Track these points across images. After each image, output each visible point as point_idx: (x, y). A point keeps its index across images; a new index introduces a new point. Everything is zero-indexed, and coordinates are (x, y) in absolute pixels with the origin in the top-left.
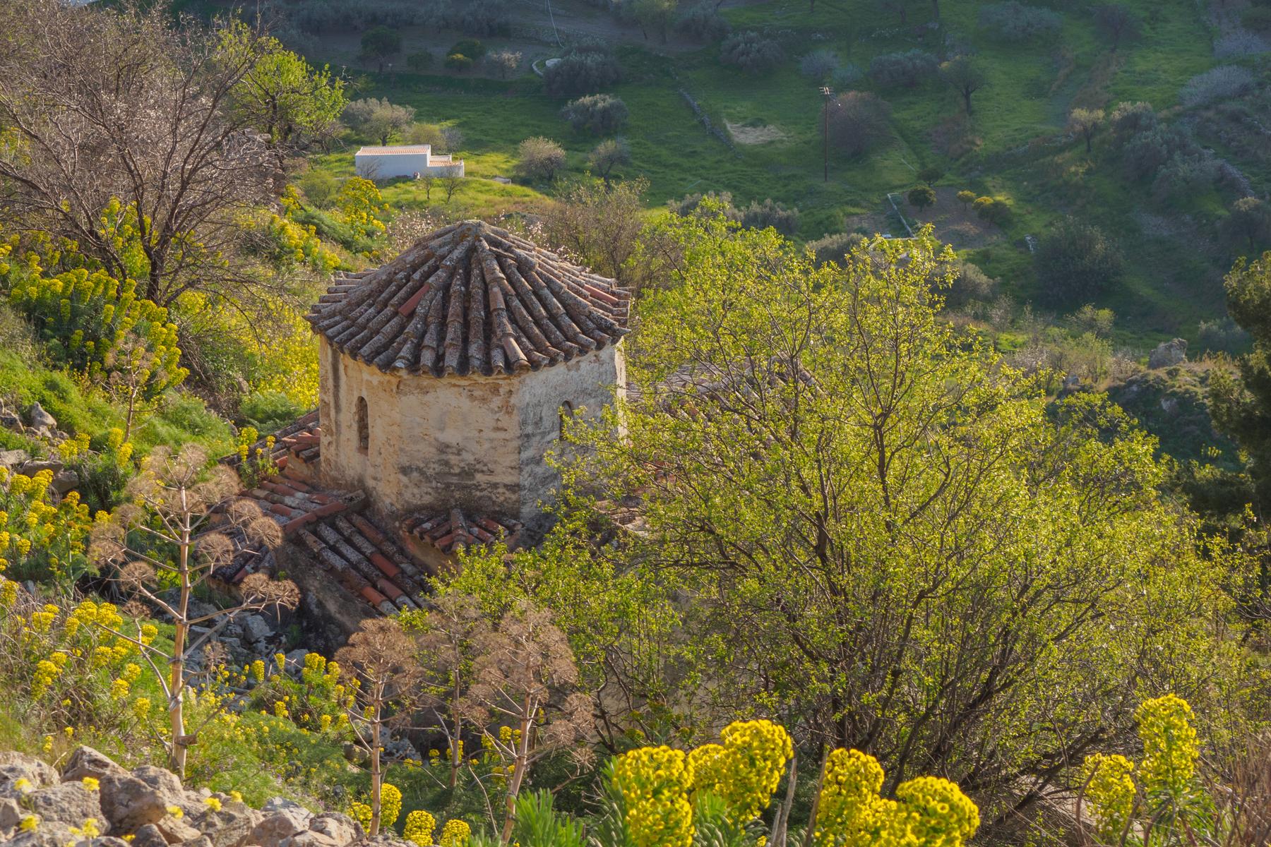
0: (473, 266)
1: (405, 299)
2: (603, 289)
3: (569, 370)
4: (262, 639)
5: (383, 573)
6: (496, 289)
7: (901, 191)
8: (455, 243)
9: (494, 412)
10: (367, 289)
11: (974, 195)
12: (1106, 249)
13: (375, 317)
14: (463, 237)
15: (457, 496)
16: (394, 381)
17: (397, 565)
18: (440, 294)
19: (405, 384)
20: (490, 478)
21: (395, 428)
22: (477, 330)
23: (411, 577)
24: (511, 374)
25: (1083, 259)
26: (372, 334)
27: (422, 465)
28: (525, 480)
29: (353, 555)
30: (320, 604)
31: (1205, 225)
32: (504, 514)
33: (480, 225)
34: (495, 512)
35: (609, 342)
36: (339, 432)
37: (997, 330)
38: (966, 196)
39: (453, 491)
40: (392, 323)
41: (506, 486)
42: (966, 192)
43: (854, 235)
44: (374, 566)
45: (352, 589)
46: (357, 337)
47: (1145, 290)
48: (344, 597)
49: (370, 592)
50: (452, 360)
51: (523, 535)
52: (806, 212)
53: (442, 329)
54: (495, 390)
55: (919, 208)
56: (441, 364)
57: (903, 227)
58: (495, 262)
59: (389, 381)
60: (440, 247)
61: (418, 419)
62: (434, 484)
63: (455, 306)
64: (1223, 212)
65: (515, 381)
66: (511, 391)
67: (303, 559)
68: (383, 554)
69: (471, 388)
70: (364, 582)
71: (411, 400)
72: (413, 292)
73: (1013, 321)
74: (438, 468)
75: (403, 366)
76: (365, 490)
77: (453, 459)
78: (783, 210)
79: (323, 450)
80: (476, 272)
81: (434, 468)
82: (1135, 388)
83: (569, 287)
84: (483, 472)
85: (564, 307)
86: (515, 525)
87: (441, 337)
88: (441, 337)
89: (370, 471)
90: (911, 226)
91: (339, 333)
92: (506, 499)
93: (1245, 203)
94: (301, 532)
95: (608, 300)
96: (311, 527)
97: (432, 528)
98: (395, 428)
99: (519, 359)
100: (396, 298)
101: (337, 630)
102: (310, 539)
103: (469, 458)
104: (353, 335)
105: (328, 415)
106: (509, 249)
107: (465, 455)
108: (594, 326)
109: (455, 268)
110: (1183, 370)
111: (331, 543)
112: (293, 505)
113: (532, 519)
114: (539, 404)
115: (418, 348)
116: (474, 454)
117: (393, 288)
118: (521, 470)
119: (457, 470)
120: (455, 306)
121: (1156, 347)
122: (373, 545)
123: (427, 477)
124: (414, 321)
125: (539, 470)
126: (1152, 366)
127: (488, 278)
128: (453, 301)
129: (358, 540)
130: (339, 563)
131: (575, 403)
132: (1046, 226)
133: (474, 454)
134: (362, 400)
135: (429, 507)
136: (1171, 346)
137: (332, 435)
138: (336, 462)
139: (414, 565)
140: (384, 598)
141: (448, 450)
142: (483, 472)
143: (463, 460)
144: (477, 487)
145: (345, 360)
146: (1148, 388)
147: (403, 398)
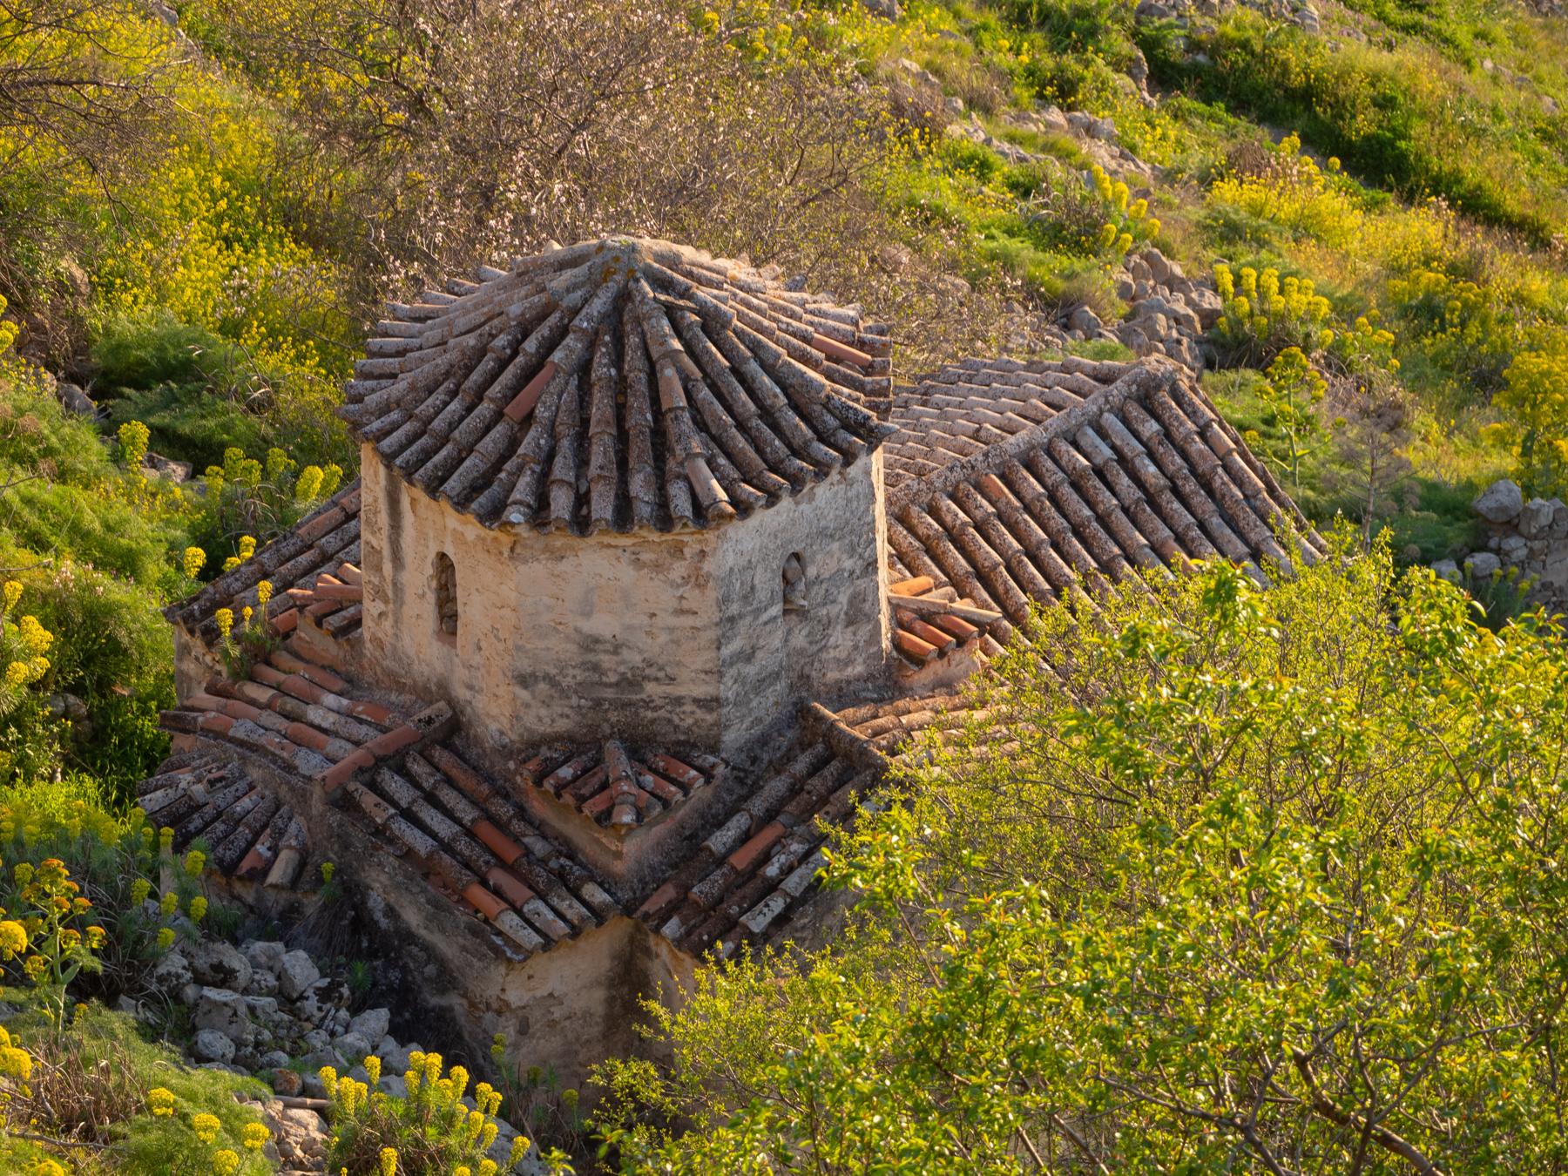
0: (628, 328)
4: (310, 993)
5: (494, 854)
6: (670, 372)
13: (462, 419)
14: (607, 274)
16: (505, 539)
17: (517, 840)
18: (574, 381)
19: (524, 547)
20: (669, 689)
21: (506, 612)
22: (640, 447)
23: (543, 862)
24: (704, 527)
26: (460, 451)
27: (553, 671)
28: (728, 689)
29: (444, 828)
30: (391, 912)
32: (694, 746)
34: (679, 743)
41: (696, 701)
45: (445, 887)
48: (436, 905)
49: (478, 894)
50: (602, 506)
53: (581, 445)
54: (678, 551)
56: (584, 511)
59: (495, 539)
60: (568, 291)
62: (574, 701)
63: (601, 406)
65: (710, 535)
66: (703, 552)
67: (359, 837)
68: (491, 818)
69: (637, 549)
70: (466, 876)
71: (536, 570)
72: (529, 374)
74: (581, 675)
75: (521, 518)
76: (451, 702)
77: (607, 661)
79: (367, 622)
80: (633, 340)
81: (577, 675)
84: (657, 679)
85: (784, 389)
86: (713, 766)
87: (582, 462)
88: (582, 462)
89: (461, 674)
91: (402, 448)
92: (697, 721)
94: (351, 786)
96: (367, 776)
97: (576, 778)
98: (506, 612)
99: (716, 501)
102: (368, 800)
103: (636, 659)
104: (427, 454)
107: (626, 654)
109: (596, 333)
111: (404, 804)
112: (325, 725)
113: (740, 750)
115: (543, 483)
116: (640, 652)
117: (488, 363)
118: (721, 674)
119: (613, 678)
120: (601, 406)
122: (474, 803)
123: (563, 691)
124: (532, 433)
125: (750, 670)
127: (655, 352)
128: (595, 390)
129: (448, 796)
131: (807, 554)
133: (640, 652)
134: (442, 556)
135: (569, 738)
137: (386, 602)
138: (395, 648)
139: (544, 837)
140: (504, 905)
141: (600, 647)
142: (657, 679)
143: (623, 662)
144: (647, 704)
145: (409, 495)
147: (522, 568)
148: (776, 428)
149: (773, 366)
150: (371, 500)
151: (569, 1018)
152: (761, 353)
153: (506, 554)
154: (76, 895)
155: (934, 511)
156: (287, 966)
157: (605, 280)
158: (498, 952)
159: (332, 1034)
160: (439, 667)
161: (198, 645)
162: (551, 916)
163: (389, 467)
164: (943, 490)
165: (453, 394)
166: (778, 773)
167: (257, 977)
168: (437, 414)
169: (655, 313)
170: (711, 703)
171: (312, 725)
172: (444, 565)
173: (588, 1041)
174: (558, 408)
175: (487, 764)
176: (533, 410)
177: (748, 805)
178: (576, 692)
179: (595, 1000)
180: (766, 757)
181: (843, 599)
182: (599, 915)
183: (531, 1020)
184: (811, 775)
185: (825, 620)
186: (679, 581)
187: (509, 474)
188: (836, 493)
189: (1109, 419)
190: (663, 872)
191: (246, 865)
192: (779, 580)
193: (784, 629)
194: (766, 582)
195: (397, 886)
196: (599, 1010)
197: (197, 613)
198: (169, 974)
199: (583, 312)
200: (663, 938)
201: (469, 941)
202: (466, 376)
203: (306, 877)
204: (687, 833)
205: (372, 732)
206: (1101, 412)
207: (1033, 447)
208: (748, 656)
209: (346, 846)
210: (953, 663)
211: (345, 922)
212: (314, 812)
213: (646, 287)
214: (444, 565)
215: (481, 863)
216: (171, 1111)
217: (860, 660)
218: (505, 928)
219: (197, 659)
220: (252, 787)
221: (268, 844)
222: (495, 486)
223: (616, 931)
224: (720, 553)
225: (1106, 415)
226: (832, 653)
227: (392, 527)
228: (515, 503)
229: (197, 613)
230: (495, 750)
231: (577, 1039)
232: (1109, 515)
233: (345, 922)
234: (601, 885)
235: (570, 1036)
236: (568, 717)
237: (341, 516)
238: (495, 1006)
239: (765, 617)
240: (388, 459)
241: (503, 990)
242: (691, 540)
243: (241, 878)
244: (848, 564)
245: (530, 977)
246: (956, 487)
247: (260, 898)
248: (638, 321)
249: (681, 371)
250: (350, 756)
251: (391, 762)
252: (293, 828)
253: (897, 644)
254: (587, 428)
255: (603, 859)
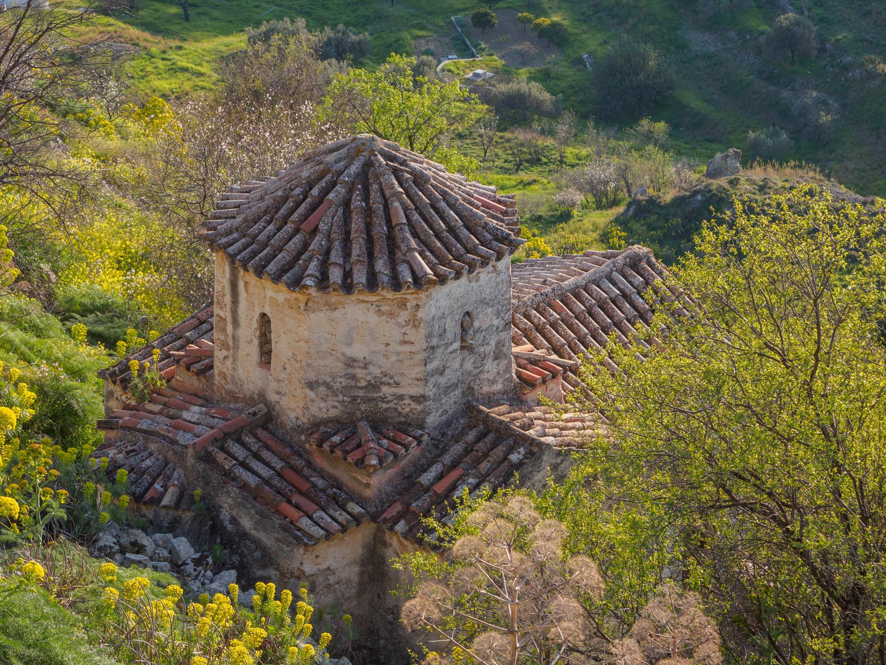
0: (371, 181)
1: (306, 216)
2: (489, 198)
3: (470, 282)
4: (189, 561)
5: (295, 487)
6: (396, 204)
7: (463, 14)
8: (351, 159)
9: (400, 326)
10: (263, 205)
11: (532, 16)
12: (658, 65)
13: (275, 234)
14: (358, 152)
15: (363, 409)
16: (302, 298)
17: (307, 479)
18: (341, 210)
19: (314, 302)
20: (395, 390)
21: (302, 344)
22: (380, 245)
23: (323, 491)
24: (420, 289)
25: (637, 75)
26: (275, 251)
27: (328, 379)
28: (430, 391)
29: (265, 472)
30: (234, 521)
31: (749, 40)
32: (410, 425)
33: (373, 139)
34: (400, 423)
35: (507, 253)
36: (236, 347)
37: (562, 143)
38: (525, 17)
39: (359, 404)
40: (295, 240)
41: (411, 397)
42: (525, 14)
43: (425, 57)
44: (285, 479)
45: (267, 504)
46: (261, 255)
47: (695, 103)
48: (261, 514)
49: (286, 508)
50: (360, 276)
51: (427, 445)
52: (376, 35)
53: (345, 245)
54: (403, 304)
55: (481, 29)
56: (349, 281)
57: (467, 48)
58: (393, 177)
59: (296, 299)
60: (336, 162)
61: (325, 335)
62: (340, 398)
63: (357, 223)
64: (764, 27)
65: (422, 295)
66: (418, 305)
67: (215, 477)
70: (279, 498)
71: (319, 317)
72: (313, 208)
73: (576, 135)
75: (313, 284)
76: (267, 404)
77: (360, 373)
78: (355, 34)
79: (217, 364)
80: (375, 187)
81: (341, 382)
82: (699, 197)
83: (464, 199)
84: (389, 384)
85: (461, 218)
86: (422, 435)
87: (347, 254)
88: (347, 254)
89: (273, 385)
90: (475, 47)
91: (240, 252)
93: (786, 19)
94: (210, 449)
95: (497, 209)
96: (219, 443)
97: (342, 442)
99: (426, 274)
100: (295, 215)
101: (253, 546)
102: (220, 456)
103: (377, 372)
104: (255, 254)
105: (224, 330)
106: (404, 163)
107: (371, 369)
108: (491, 237)
109: (353, 184)
110: (742, 179)
111: (241, 459)
112: (192, 420)
113: (435, 428)
114: (443, 316)
115: (325, 265)
116: (380, 367)
118: (427, 381)
119: (363, 383)
120: (357, 223)
121: (712, 157)
122: (282, 459)
124: (317, 238)
125: (442, 380)
126: (712, 174)
127: (387, 193)
129: (266, 455)
130: (252, 480)
131: (474, 313)
132: (601, 44)
133: (380, 367)
134: (263, 315)
135: (336, 421)
136: (727, 156)
137: (228, 349)
138: (233, 376)
140: (302, 514)
142: (389, 384)
143: (369, 374)
144: (383, 399)
146: (711, 197)
147: (312, 315)
148: (457, 238)
149: (454, 205)
150: (220, 288)
151: (338, 583)
152: (447, 197)
153: (302, 308)
154: (51, 468)
155: (527, 316)
156: (175, 545)
157: (357, 156)
158: (299, 540)
159: (203, 584)
160: (260, 384)
161: (117, 390)
162: (329, 520)
163: (233, 262)
164: (532, 307)
165: (269, 222)
166: (457, 442)
167: (157, 551)
168: (260, 233)
169: (387, 172)
170: (420, 399)
171: (185, 420)
172: (265, 321)
173: (349, 598)
174: (332, 225)
175: (288, 438)
176: (317, 226)
177: (442, 458)
178: (341, 392)
179: (352, 573)
180: (450, 433)
181: (493, 343)
182: (357, 520)
183: (317, 583)
184: (476, 442)
185: (483, 355)
186: (404, 323)
187: (304, 261)
188: (491, 278)
189: (616, 276)
190: (393, 497)
191: (148, 496)
192: (459, 327)
193: (461, 357)
194: (452, 328)
195: (238, 505)
196: (355, 579)
197: (117, 372)
198: (105, 546)
199: (346, 172)
200: (396, 533)
201: (281, 535)
202: (277, 212)
203: (184, 501)
204: (407, 475)
205: (221, 421)
206: (612, 271)
207: (577, 287)
208: (441, 372)
209: (207, 483)
210: (549, 389)
211: (207, 528)
212: (188, 464)
213: (382, 159)
214: (265, 321)
215: (287, 490)
216: (115, 578)
217: (500, 381)
218: (303, 526)
219: (117, 398)
220: (151, 454)
221: (161, 484)
222: (296, 268)
223: (366, 531)
224: (427, 306)
225: (614, 273)
226: (486, 376)
227: (233, 302)
228: (308, 276)
229: (117, 372)
230: (293, 429)
231: (343, 596)
232: (621, 323)
233: (207, 528)
234: (357, 503)
235: (339, 594)
236: (336, 407)
237: (197, 322)
238: (296, 574)
239: (451, 349)
240: (232, 258)
241: (302, 564)
242: (410, 296)
243: (145, 503)
244: (496, 322)
245: (317, 557)
246: (538, 305)
247: (156, 515)
248: (377, 177)
249: (403, 204)
250: (207, 433)
251: (233, 436)
252: (176, 475)
253: (519, 375)
254: (349, 236)
255: (359, 489)
